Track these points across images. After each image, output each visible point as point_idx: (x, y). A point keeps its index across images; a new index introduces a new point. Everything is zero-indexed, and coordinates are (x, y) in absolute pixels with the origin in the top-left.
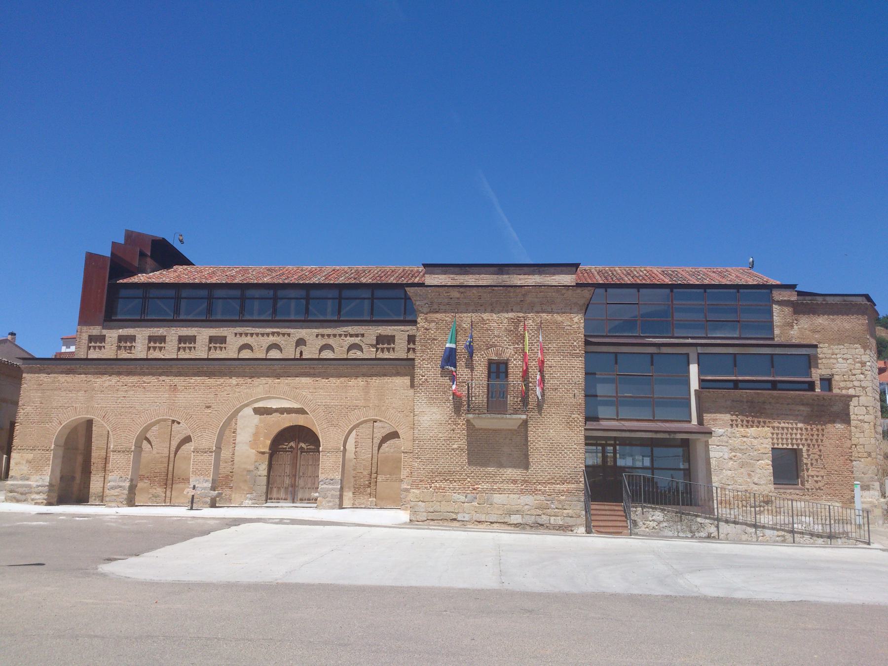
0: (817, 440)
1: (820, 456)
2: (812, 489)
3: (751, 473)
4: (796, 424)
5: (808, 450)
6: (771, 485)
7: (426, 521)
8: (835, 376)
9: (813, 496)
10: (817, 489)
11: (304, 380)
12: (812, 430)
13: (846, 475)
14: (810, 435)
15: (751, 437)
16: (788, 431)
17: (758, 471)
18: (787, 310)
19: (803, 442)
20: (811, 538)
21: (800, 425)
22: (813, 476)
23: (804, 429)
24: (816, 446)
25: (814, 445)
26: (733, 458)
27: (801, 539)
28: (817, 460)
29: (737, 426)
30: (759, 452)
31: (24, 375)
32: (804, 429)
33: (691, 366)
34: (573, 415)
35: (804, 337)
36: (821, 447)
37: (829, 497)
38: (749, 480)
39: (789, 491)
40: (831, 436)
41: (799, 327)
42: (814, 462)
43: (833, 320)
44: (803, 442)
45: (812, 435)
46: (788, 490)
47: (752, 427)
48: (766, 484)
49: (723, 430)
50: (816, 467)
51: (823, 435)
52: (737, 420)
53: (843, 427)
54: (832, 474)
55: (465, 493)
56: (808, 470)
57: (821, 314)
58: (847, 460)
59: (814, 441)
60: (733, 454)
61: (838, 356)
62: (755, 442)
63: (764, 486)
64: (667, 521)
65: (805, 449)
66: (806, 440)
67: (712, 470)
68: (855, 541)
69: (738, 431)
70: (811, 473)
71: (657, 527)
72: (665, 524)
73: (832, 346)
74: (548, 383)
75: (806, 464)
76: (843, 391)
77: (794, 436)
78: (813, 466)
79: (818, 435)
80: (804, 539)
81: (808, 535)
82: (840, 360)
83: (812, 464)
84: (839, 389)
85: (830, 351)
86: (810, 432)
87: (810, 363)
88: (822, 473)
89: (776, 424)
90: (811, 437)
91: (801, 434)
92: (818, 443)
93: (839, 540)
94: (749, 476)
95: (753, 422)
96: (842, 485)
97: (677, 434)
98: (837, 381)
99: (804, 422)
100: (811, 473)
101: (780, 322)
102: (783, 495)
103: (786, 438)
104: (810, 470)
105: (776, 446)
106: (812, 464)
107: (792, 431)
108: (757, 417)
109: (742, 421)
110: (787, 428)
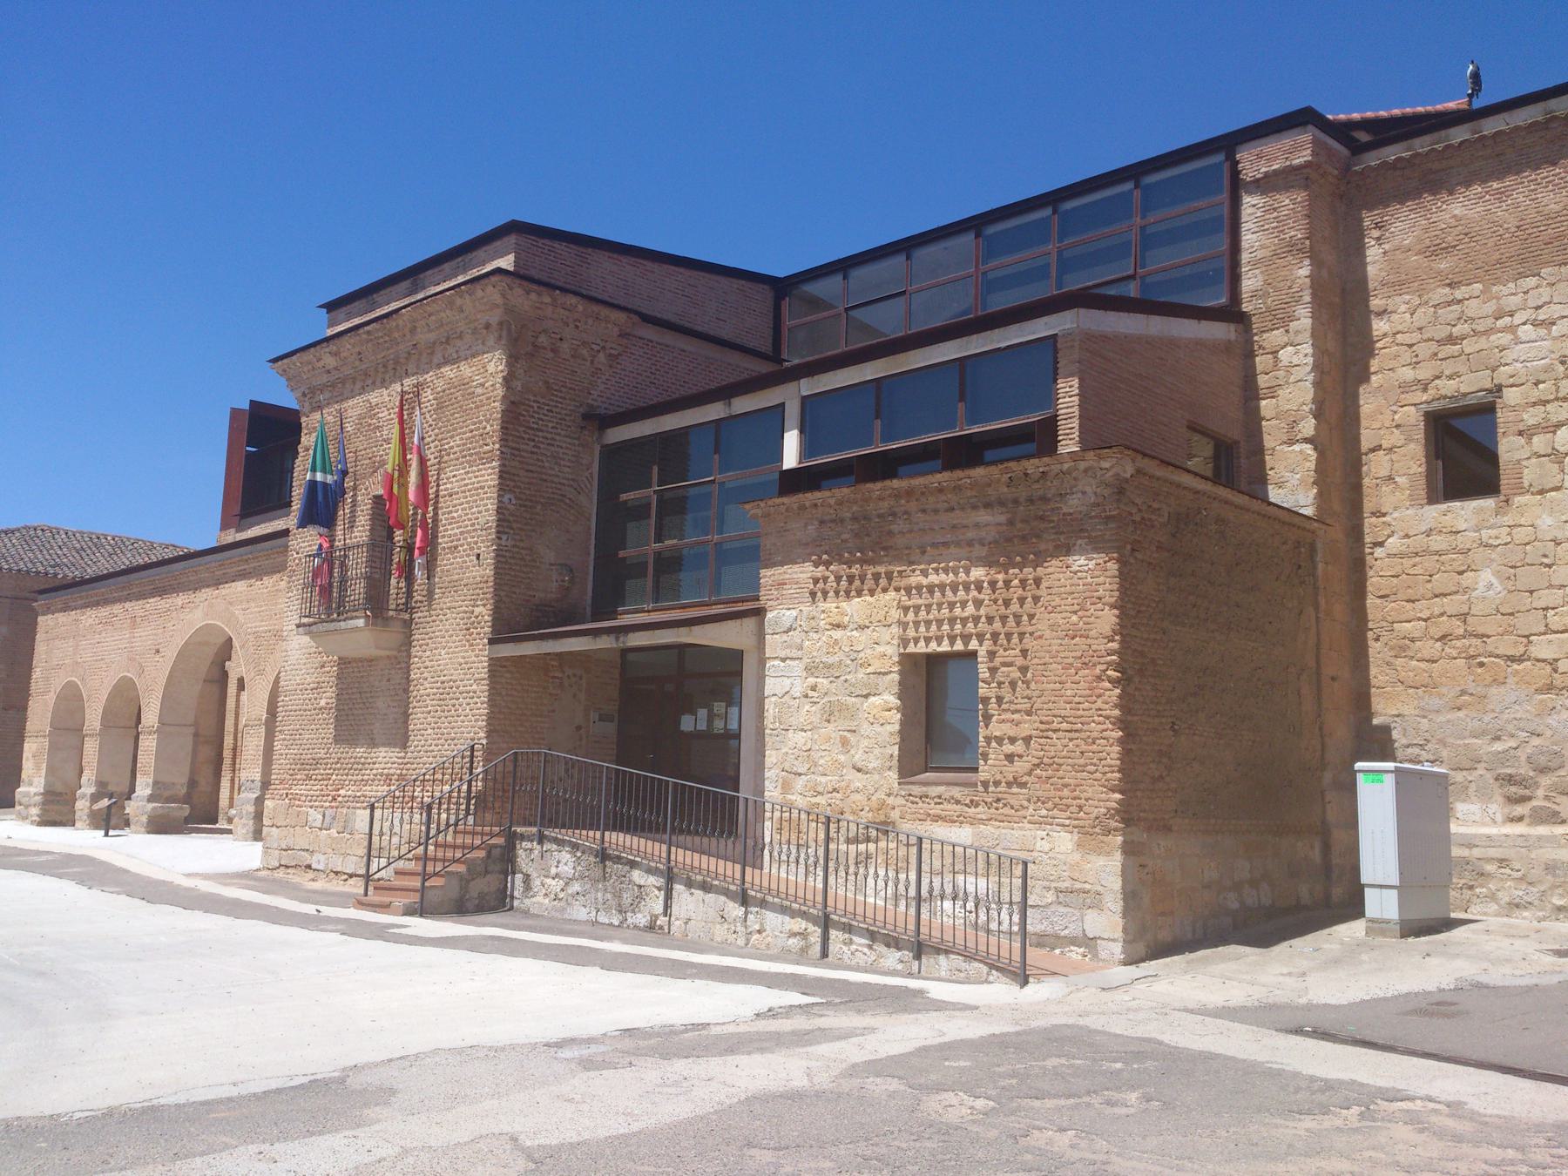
0: (1017, 617)
1: (1024, 670)
2: (997, 784)
3: (848, 735)
4: (967, 573)
5: (992, 655)
6: (891, 773)
7: (278, 868)
8: (1504, 390)
9: (997, 809)
10: (1009, 785)
11: (240, 586)
12: (1007, 583)
13: (1095, 734)
14: (1000, 602)
15: (851, 626)
16: (944, 595)
17: (865, 729)
18: (1287, 201)
19: (983, 626)
20: (870, 947)
21: (978, 573)
22: (1000, 740)
23: (985, 585)
24: (1015, 639)
25: (1009, 636)
26: (811, 693)
27: (845, 948)
28: (1013, 684)
29: (825, 594)
30: (870, 670)
31: (40, 618)
32: (985, 585)
33: (786, 435)
34: (476, 609)
35: (1403, 277)
36: (1028, 642)
37: (1044, 812)
38: (842, 758)
39: (934, 791)
40: (1057, 601)
41: (1386, 247)
42: (1006, 692)
43: (1501, 195)
44: (983, 626)
45: (1007, 603)
46: (934, 788)
47: (859, 594)
48: (880, 771)
49: (794, 613)
50: (1013, 707)
51: (1036, 599)
52: (825, 579)
53: (1092, 565)
54: (1055, 731)
55: (322, 807)
56: (988, 718)
57: (1457, 184)
58: (1099, 679)
59: (1011, 621)
60: (811, 680)
61: (1519, 318)
62: (862, 638)
63: (876, 777)
64: (582, 878)
65: (982, 652)
66: (990, 620)
67: (767, 731)
68: (985, 969)
69: (823, 611)
70: (996, 729)
71: (561, 895)
72: (576, 887)
73: (1495, 289)
74: (444, 536)
75: (986, 700)
76: (1535, 439)
77: (958, 611)
78: (1004, 706)
79: (1022, 601)
80: (854, 947)
81: (861, 936)
82: (1526, 331)
83: (1000, 700)
84: (1520, 433)
85: (1490, 307)
86: (1001, 594)
87: (1056, 369)
88: (1026, 729)
89: (916, 579)
90: (1003, 610)
91: (978, 604)
92: (1022, 629)
93: (942, 958)
94: (843, 745)
95: (862, 579)
96: (1082, 770)
97: (631, 635)
98: (1514, 409)
99: (989, 563)
100: (996, 729)
101: (1262, 247)
102: (921, 804)
103: (937, 621)
104: (994, 719)
105: (911, 649)
106: (1000, 700)
107: (955, 593)
108: (872, 562)
109: (838, 579)
110: (942, 587)
